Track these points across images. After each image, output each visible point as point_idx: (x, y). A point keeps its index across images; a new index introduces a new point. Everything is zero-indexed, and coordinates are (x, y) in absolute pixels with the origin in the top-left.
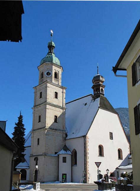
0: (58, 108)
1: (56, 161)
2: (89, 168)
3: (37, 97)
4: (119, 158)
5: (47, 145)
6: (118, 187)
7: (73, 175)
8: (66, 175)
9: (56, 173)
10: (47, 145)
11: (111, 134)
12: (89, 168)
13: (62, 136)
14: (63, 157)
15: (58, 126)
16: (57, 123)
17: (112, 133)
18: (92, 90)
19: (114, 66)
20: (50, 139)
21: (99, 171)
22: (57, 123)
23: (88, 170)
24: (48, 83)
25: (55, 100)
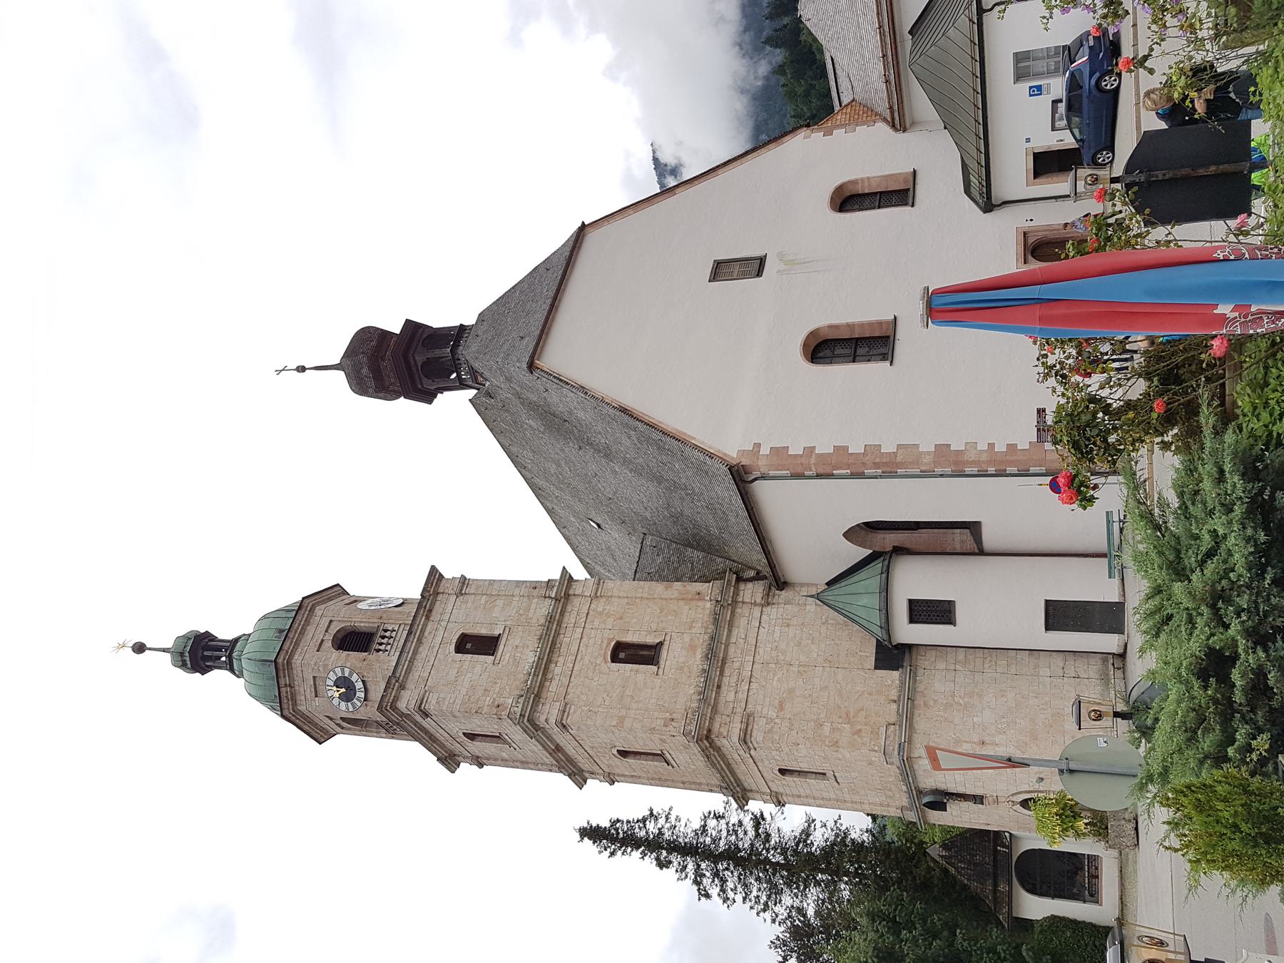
0: (557, 634)
1: (942, 665)
2: (991, 446)
3: (504, 755)
4: (904, 203)
5: (827, 729)
6: (1283, 192)
7: (1090, 774)
8: (1044, 410)
9: (1045, 671)
10: (827, 729)
11: (720, 270)
13: (757, 611)
14: (912, 621)
15: (687, 638)
16: (661, 644)
17: (718, 265)
18: (444, 399)
19: (586, 224)
20: (781, 708)
21: (997, 801)
22: (661, 644)
23: (1012, 447)
24: (396, 699)
25: (509, 648)
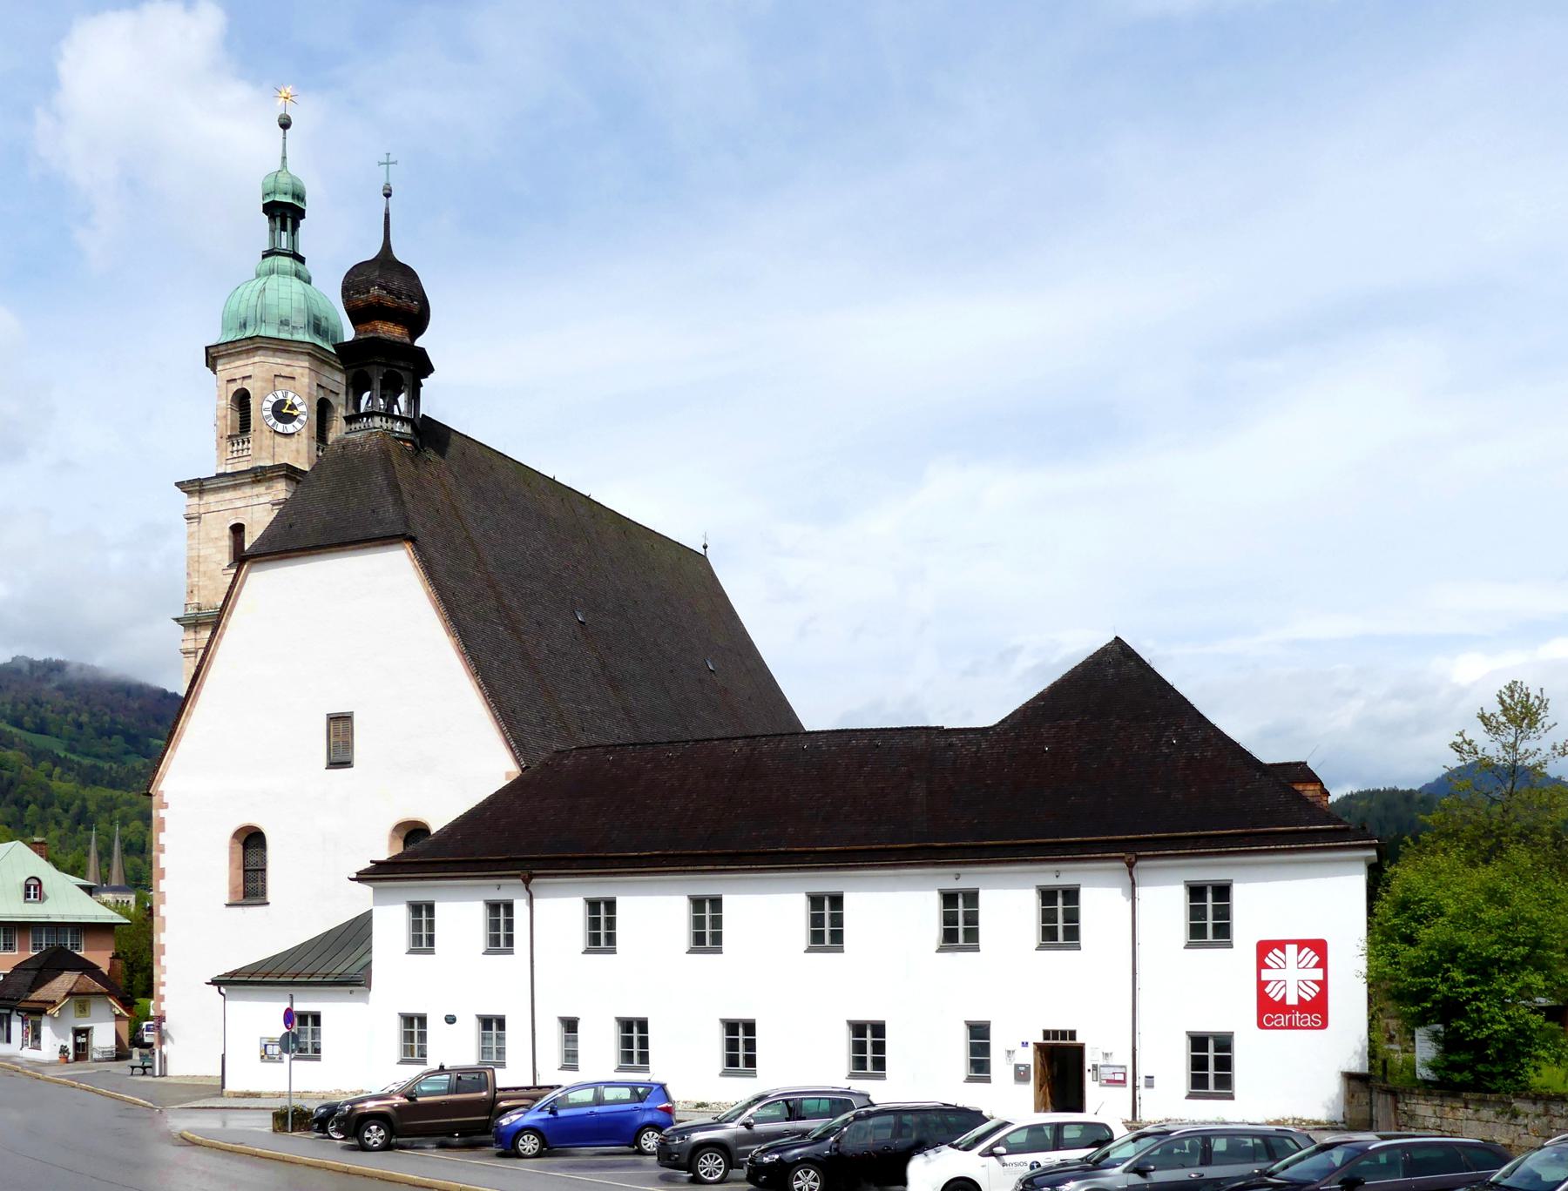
2: (163, 984)
12: (163, 984)
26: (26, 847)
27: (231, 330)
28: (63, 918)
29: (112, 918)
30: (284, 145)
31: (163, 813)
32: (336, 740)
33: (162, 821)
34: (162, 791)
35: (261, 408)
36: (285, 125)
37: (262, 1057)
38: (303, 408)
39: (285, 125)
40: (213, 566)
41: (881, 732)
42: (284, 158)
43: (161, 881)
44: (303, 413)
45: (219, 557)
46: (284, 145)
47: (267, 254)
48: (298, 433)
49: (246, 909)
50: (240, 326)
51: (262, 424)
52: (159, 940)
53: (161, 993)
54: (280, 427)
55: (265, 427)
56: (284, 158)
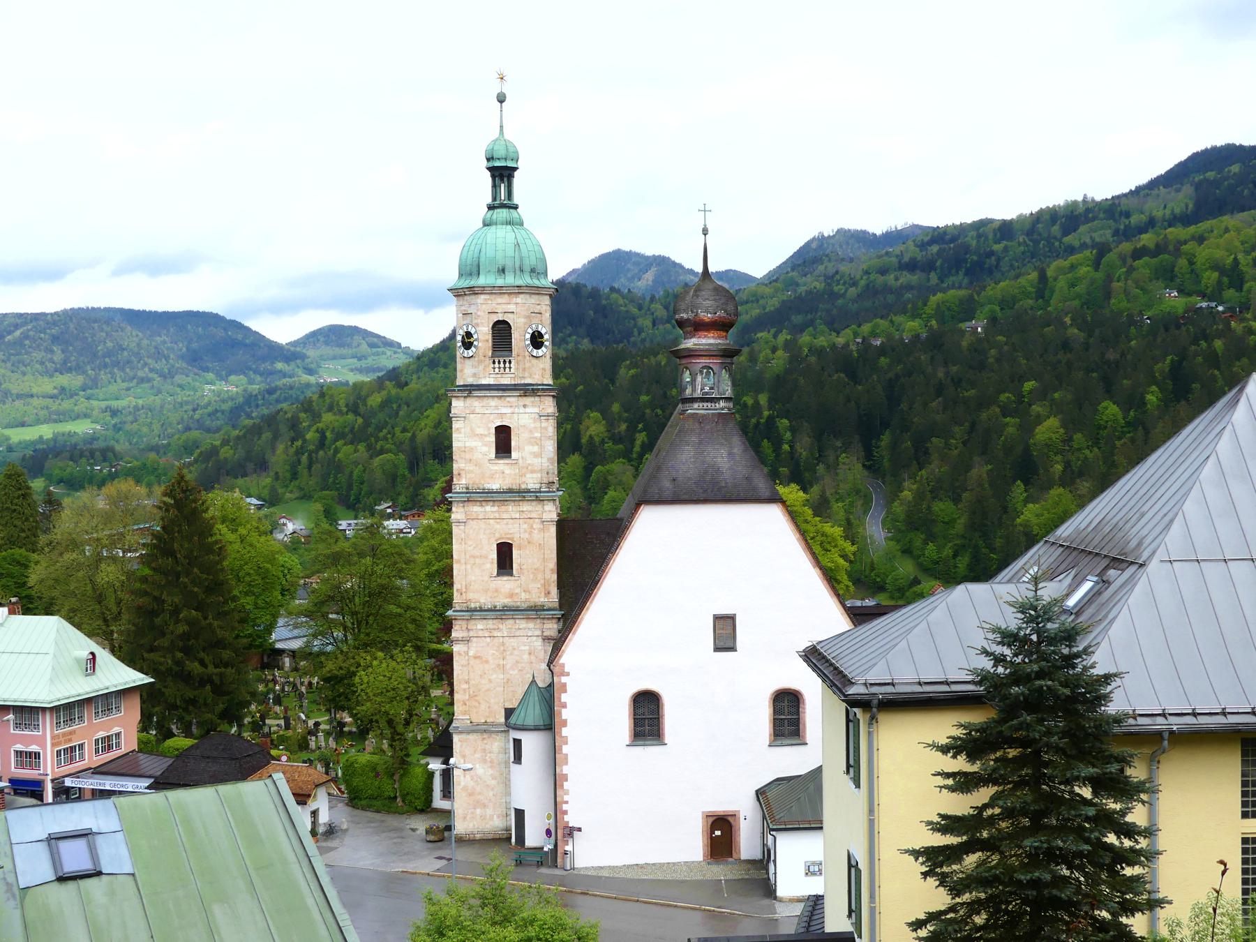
2: (564, 706)
12: (564, 706)
15: (517, 591)
26: (82, 635)
27: (489, 271)
28: (116, 687)
29: (143, 680)
30: (501, 117)
31: (564, 679)
32: (353, 525)
33: (564, 685)
34: (564, 664)
35: (520, 338)
36: (501, 99)
37: (807, 874)
38: (546, 337)
39: (501, 99)
40: (480, 456)
41: (702, 496)
42: (501, 127)
43: (563, 729)
44: (547, 340)
45: (485, 449)
46: (501, 117)
47: (491, 208)
48: (544, 356)
49: (646, 747)
50: (498, 271)
51: (524, 351)
52: (562, 771)
53: (564, 809)
54: (535, 352)
55: (527, 353)
56: (501, 127)
